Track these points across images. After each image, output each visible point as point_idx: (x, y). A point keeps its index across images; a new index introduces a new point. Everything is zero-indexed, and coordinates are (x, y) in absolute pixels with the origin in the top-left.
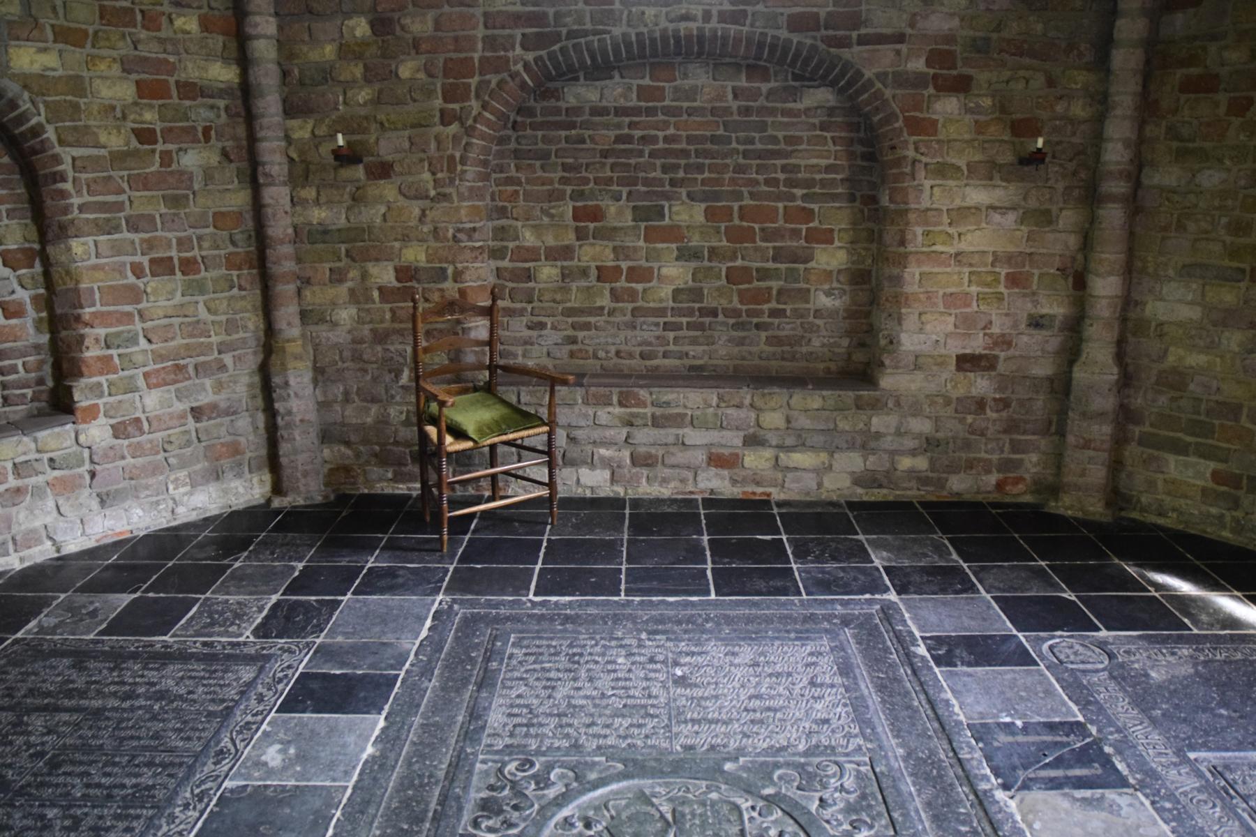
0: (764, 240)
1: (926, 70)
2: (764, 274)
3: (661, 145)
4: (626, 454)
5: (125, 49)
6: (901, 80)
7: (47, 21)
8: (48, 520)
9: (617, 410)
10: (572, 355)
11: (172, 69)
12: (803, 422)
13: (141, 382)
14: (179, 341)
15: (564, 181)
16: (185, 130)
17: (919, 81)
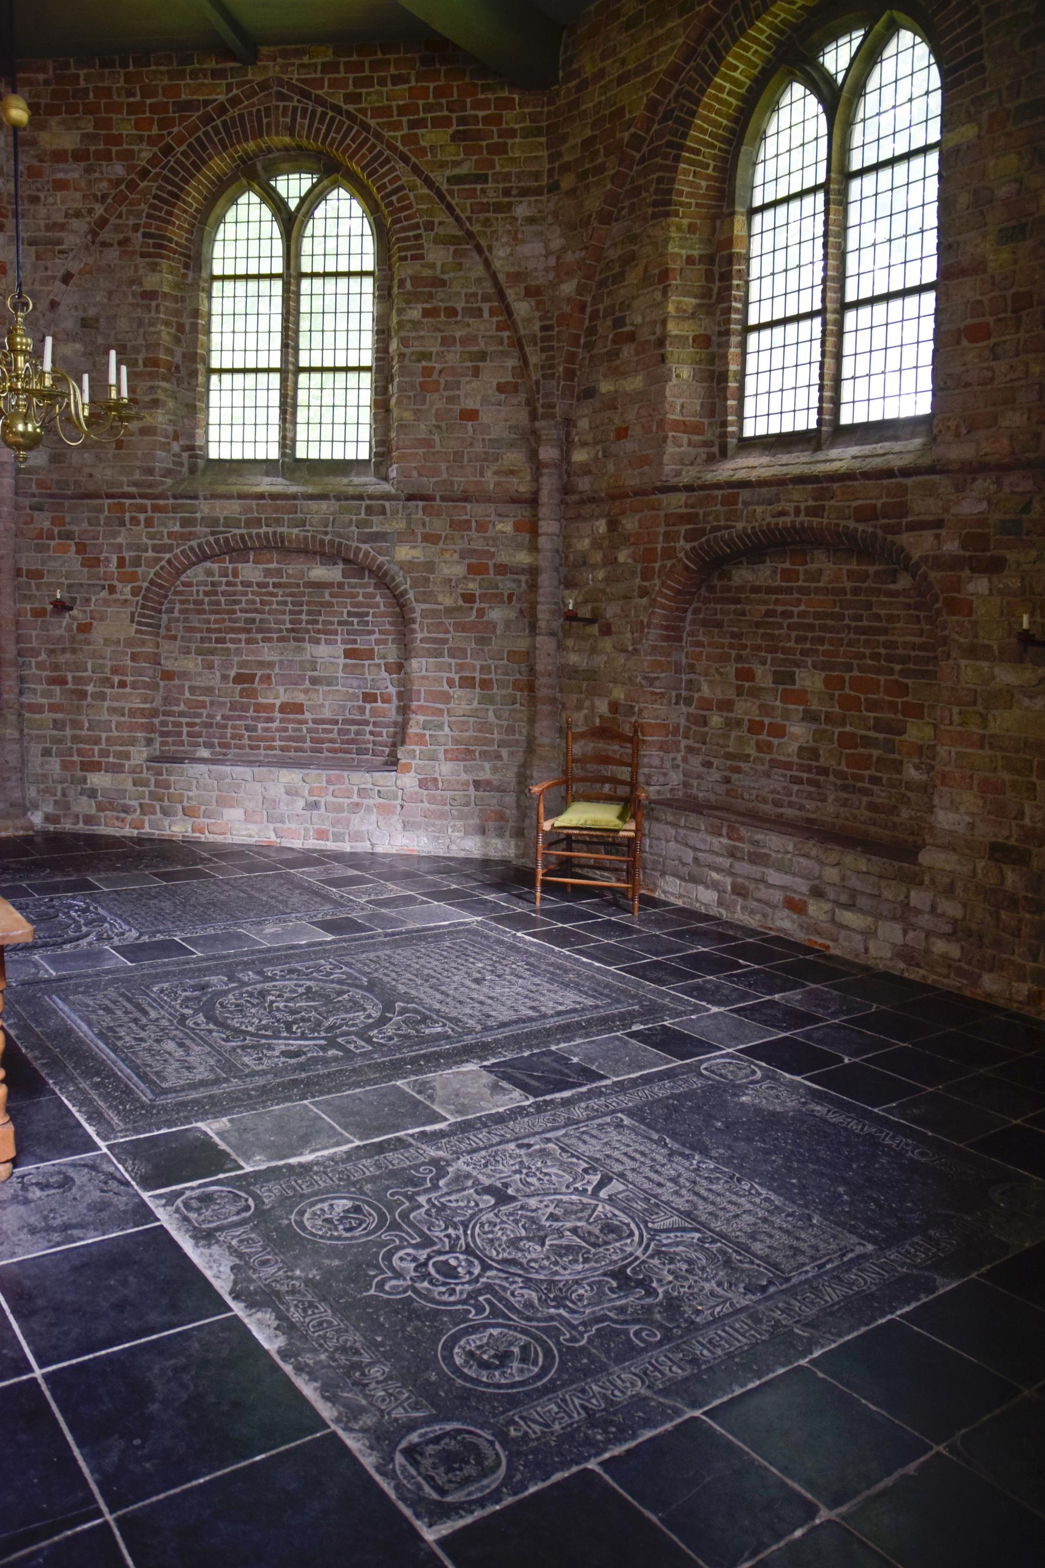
0: (868, 710)
1: (962, 553)
2: (867, 742)
3: (795, 619)
4: (728, 881)
5: (463, 545)
6: (938, 562)
7: (419, 531)
8: (371, 828)
9: (725, 841)
10: (728, 793)
11: (493, 555)
12: (854, 882)
13: (441, 756)
14: (470, 733)
15: (731, 646)
16: (496, 595)
17: (955, 563)
